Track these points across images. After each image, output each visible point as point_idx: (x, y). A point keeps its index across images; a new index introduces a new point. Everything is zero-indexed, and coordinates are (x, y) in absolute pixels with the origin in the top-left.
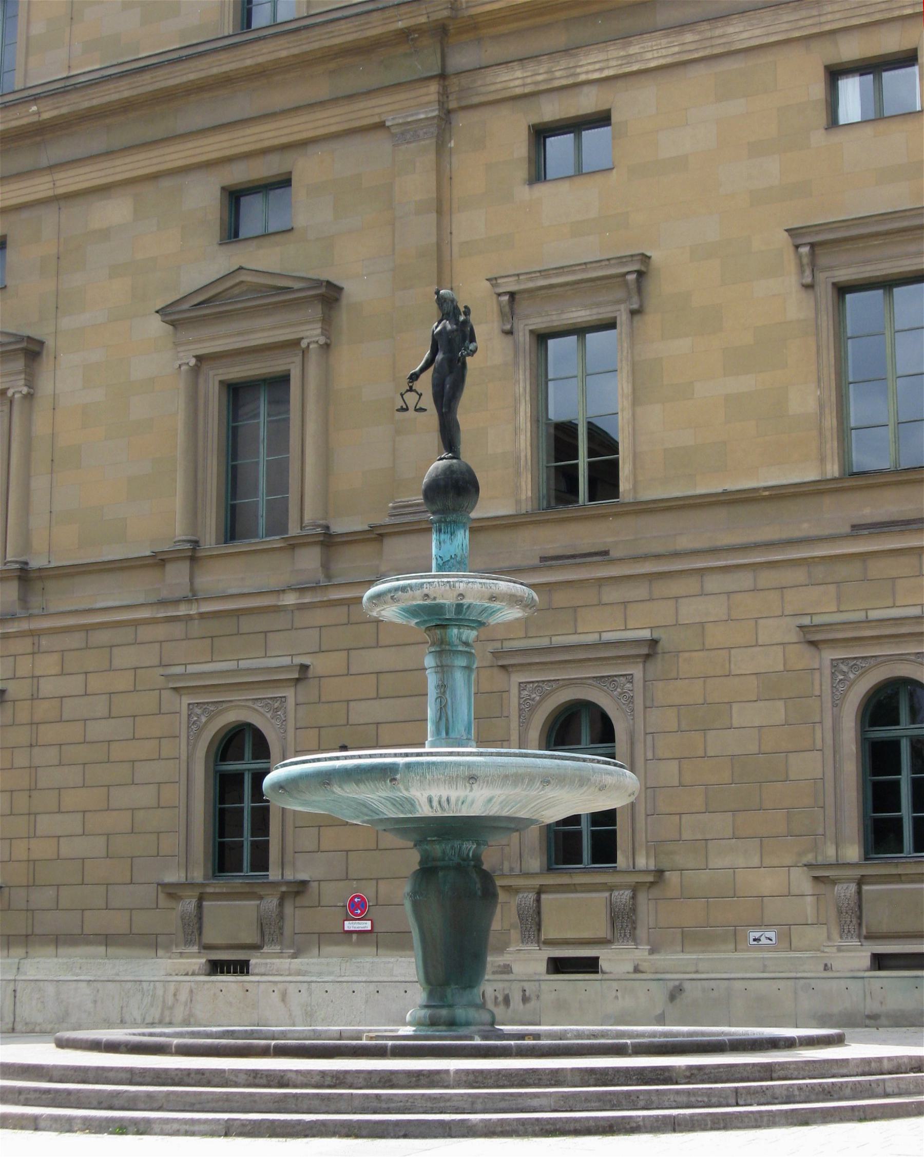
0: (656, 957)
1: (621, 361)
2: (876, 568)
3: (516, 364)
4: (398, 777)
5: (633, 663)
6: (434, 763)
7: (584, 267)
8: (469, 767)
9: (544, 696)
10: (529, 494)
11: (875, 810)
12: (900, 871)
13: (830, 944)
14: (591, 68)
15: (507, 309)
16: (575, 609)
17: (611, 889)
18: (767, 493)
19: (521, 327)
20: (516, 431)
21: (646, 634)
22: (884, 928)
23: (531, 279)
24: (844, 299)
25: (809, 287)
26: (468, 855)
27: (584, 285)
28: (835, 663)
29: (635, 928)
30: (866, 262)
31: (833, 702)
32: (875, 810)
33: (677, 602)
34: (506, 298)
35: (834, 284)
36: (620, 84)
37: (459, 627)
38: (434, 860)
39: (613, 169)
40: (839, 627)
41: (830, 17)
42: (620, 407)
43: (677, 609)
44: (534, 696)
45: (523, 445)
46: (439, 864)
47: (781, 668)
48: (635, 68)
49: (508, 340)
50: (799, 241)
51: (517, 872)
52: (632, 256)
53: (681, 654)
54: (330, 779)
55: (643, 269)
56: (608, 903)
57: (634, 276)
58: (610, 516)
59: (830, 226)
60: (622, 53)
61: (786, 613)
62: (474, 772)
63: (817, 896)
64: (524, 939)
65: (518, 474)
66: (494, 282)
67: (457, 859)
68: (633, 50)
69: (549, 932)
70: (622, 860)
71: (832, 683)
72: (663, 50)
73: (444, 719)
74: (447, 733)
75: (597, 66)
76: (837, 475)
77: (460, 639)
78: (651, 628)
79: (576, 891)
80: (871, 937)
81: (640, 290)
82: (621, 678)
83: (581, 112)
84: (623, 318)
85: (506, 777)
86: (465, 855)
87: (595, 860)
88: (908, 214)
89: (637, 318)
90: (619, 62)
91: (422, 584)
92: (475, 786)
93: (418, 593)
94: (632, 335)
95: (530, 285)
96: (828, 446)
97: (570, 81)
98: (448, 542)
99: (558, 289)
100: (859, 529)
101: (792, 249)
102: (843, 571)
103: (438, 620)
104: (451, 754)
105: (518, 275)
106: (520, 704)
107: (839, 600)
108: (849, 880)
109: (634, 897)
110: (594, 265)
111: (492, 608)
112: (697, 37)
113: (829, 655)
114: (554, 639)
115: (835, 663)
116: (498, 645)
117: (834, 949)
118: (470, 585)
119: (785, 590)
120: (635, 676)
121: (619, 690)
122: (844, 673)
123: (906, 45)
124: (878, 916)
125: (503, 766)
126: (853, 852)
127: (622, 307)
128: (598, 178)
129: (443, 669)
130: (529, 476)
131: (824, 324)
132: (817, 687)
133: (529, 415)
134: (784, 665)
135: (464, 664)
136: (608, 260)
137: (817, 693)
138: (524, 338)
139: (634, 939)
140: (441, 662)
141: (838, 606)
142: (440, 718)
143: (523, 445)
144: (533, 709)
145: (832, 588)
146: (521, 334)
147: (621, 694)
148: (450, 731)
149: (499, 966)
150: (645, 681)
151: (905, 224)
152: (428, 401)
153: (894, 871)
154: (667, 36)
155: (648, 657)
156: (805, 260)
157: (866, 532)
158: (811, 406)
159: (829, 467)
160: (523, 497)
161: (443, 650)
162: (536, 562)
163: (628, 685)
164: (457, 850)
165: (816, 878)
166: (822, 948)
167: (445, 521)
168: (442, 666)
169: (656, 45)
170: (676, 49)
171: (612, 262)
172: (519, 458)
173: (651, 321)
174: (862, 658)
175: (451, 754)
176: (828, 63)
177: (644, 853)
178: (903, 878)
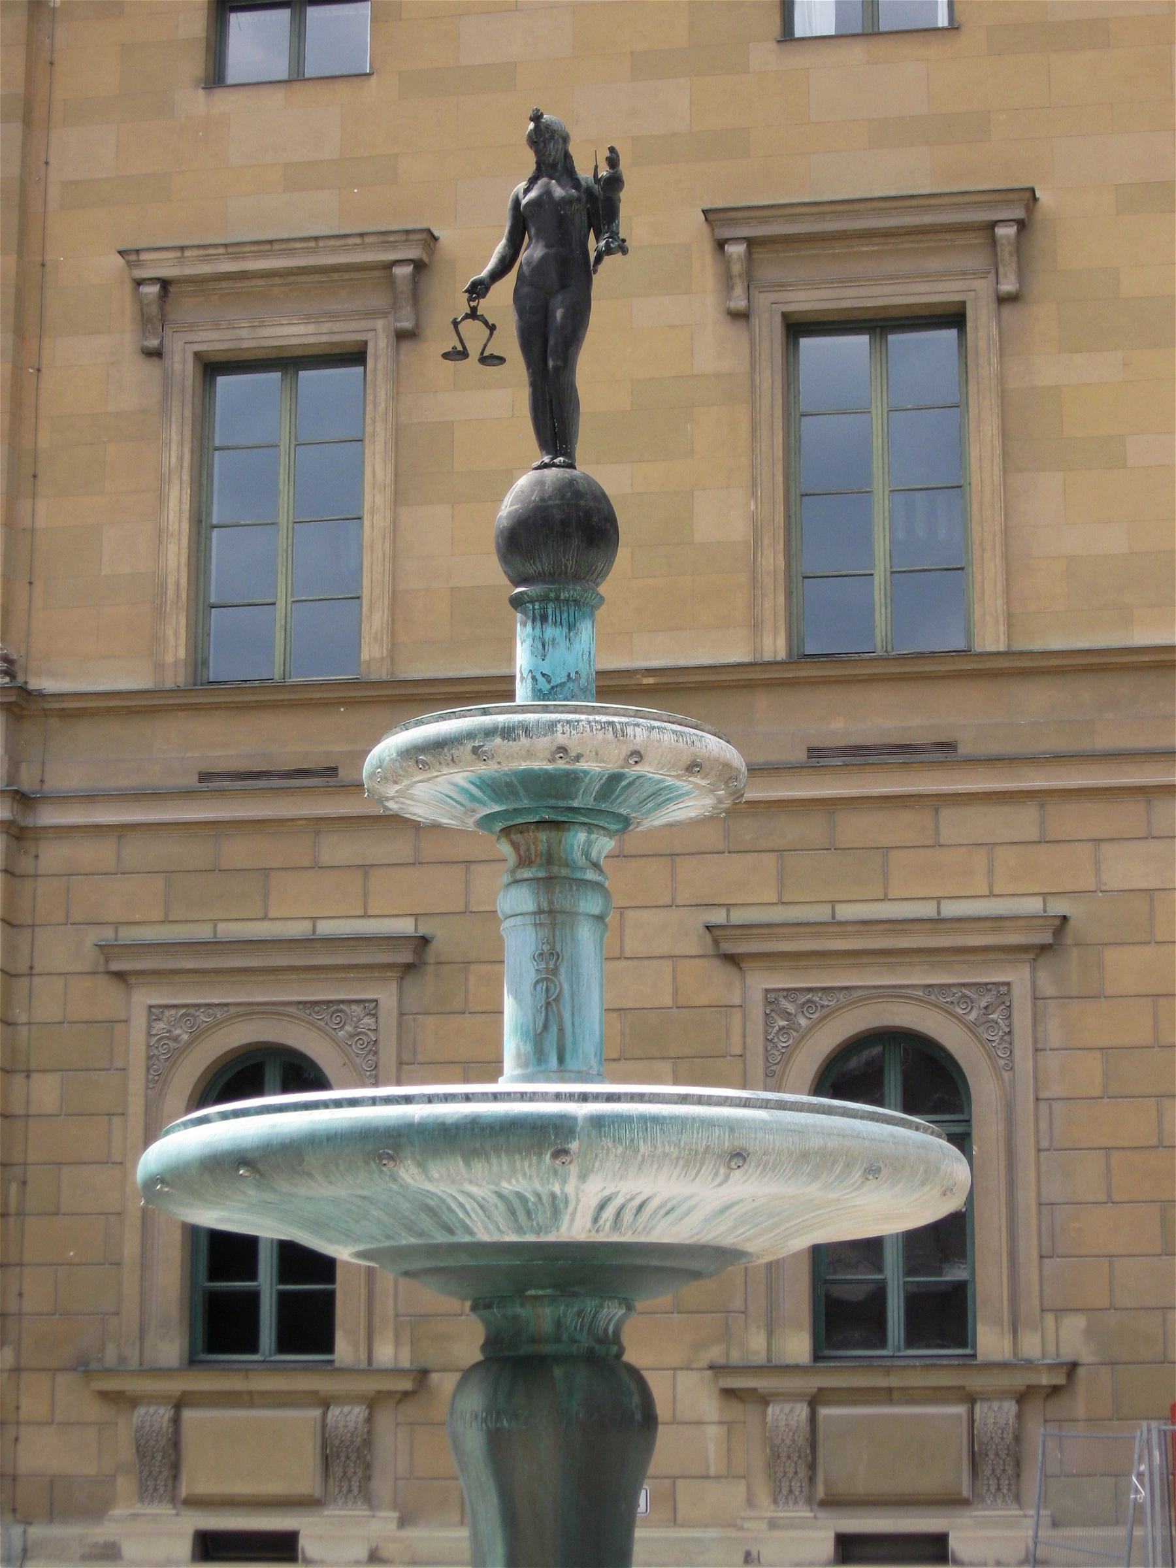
0: (411, 1533)
1: (374, 421)
2: (854, 829)
3: (165, 410)
4: (574, 1146)
5: (345, 979)
6: (655, 1119)
7: (312, 244)
8: (732, 1130)
9: (198, 1035)
10: (182, 654)
11: (212, 1277)
12: (894, 1381)
13: (752, 1514)
15: (154, 310)
16: (266, 872)
17: (325, 1403)
18: (651, 680)
19: (179, 345)
20: (160, 536)
21: (405, 926)
22: (861, 1487)
23: (206, 259)
24: (796, 344)
25: (740, 316)
26: (606, 1330)
27: (304, 278)
28: (771, 996)
29: (369, 1478)
30: (844, 282)
31: (767, 1068)
32: (212, 1277)
33: (467, 870)
34: (155, 289)
35: (785, 316)
37: (590, 828)
38: (533, 1340)
39: (370, 74)
40: (786, 931)
42: (367, 505)
43: (467, 882)
44: (177, 1032)
45: (172, 563)
46: (548, 1349)
47: (668, 1001)
49: (151, 368)
50: (726, 233)
51: (133, 1364)
52: (408, 232)
53: (473, 967)
54: (397, 1148)
55: (426, 259)
56: (319, 1428)
57: (408, 270)
58: (340, 704)
59: (788, 211)
61: (679, 902)
62: (743, 1143)
63: (729, 1426)
64: (146, 1492)
65: (160, 614)
66: (133, 257)
67: (585, 1341)
69: (195, 1481)
70: (344, 1349)
71: (766, 1033)
73: (554, 1029)
74: (561, 1060)
76: (782, 655)
77: (587, 855)
78: (416, 916)
79: (252, 1405)
80: (832, 1503)
82: (354, 1007)
84: (380, 346)
85: (805, 1155)
86: (601, 1332)
87: (286, 1343)
88: (932, 201)
89: (406, 346)
91: (553, 725)
92: (737, 1174)
93: (543, 743)
94: (396, 378)
95: (205, 269)
96: (768, 604)
98: (563, 643)
99: (254, 282)
100: (821, 757)
101: (707, 246)
102: (791, 830)
103: (544, 815)
104: (684, 1099)
105: (182, 249)
106: (149, 1047)
107: (781, 881)
108: (794, 1397)
109: (369, 1420)
110: (332, 242)
111: (678, 788)
113: (761, 981)
114: (221, 927)
115: (771, 998)
116: (108, 934)
117: (764, 1525)
118: (655, 733)
119: (678, 859)
120: (381, 1004)
121: (348, 1028)
122: (787, 1015)
124: (846, 1465)
125: (801, 1131)
126: (798, 1346)
127: (380, 324)
128: (343, 90)
129: (553, 920)
130: (183, 621)
131: (766, 385)
132: (736, 1038)
133: (186, 507)
134: (675, 994)
135: (597, 911)
136: (362, 235)
137: (737, 1050)
138: (182, 365)
139: (367, 1498)
140: (551, 902)
141: (780, 895)
142: (546, 1027)
143: (172, 563)
144: (175, 1057)
145: (769, 860)
146: (177, 358)
147: (352, 1036)
148: (568, 1056)
149: (95, 1545)
150: (401, 1014)
151: (928, 219)
153: (881, 1382)
155: (409, 968)
156: (736, 268)
157: (838, 761)
158: (738, 529)
159: (768, 642)
160: (170, 658)
161: (553, 878)
162: (192, 781)
163: (366, 1020)
164: (587, 1320)
165: (729, 1394)
166: (739, 1522)
167: (557, 599)
168: (551, 912)
171: (368, 240)
172: (163, 587)
174: (823, 989)
175: (684, 1099)
177: (391, 1335)
178: (895, 1395)
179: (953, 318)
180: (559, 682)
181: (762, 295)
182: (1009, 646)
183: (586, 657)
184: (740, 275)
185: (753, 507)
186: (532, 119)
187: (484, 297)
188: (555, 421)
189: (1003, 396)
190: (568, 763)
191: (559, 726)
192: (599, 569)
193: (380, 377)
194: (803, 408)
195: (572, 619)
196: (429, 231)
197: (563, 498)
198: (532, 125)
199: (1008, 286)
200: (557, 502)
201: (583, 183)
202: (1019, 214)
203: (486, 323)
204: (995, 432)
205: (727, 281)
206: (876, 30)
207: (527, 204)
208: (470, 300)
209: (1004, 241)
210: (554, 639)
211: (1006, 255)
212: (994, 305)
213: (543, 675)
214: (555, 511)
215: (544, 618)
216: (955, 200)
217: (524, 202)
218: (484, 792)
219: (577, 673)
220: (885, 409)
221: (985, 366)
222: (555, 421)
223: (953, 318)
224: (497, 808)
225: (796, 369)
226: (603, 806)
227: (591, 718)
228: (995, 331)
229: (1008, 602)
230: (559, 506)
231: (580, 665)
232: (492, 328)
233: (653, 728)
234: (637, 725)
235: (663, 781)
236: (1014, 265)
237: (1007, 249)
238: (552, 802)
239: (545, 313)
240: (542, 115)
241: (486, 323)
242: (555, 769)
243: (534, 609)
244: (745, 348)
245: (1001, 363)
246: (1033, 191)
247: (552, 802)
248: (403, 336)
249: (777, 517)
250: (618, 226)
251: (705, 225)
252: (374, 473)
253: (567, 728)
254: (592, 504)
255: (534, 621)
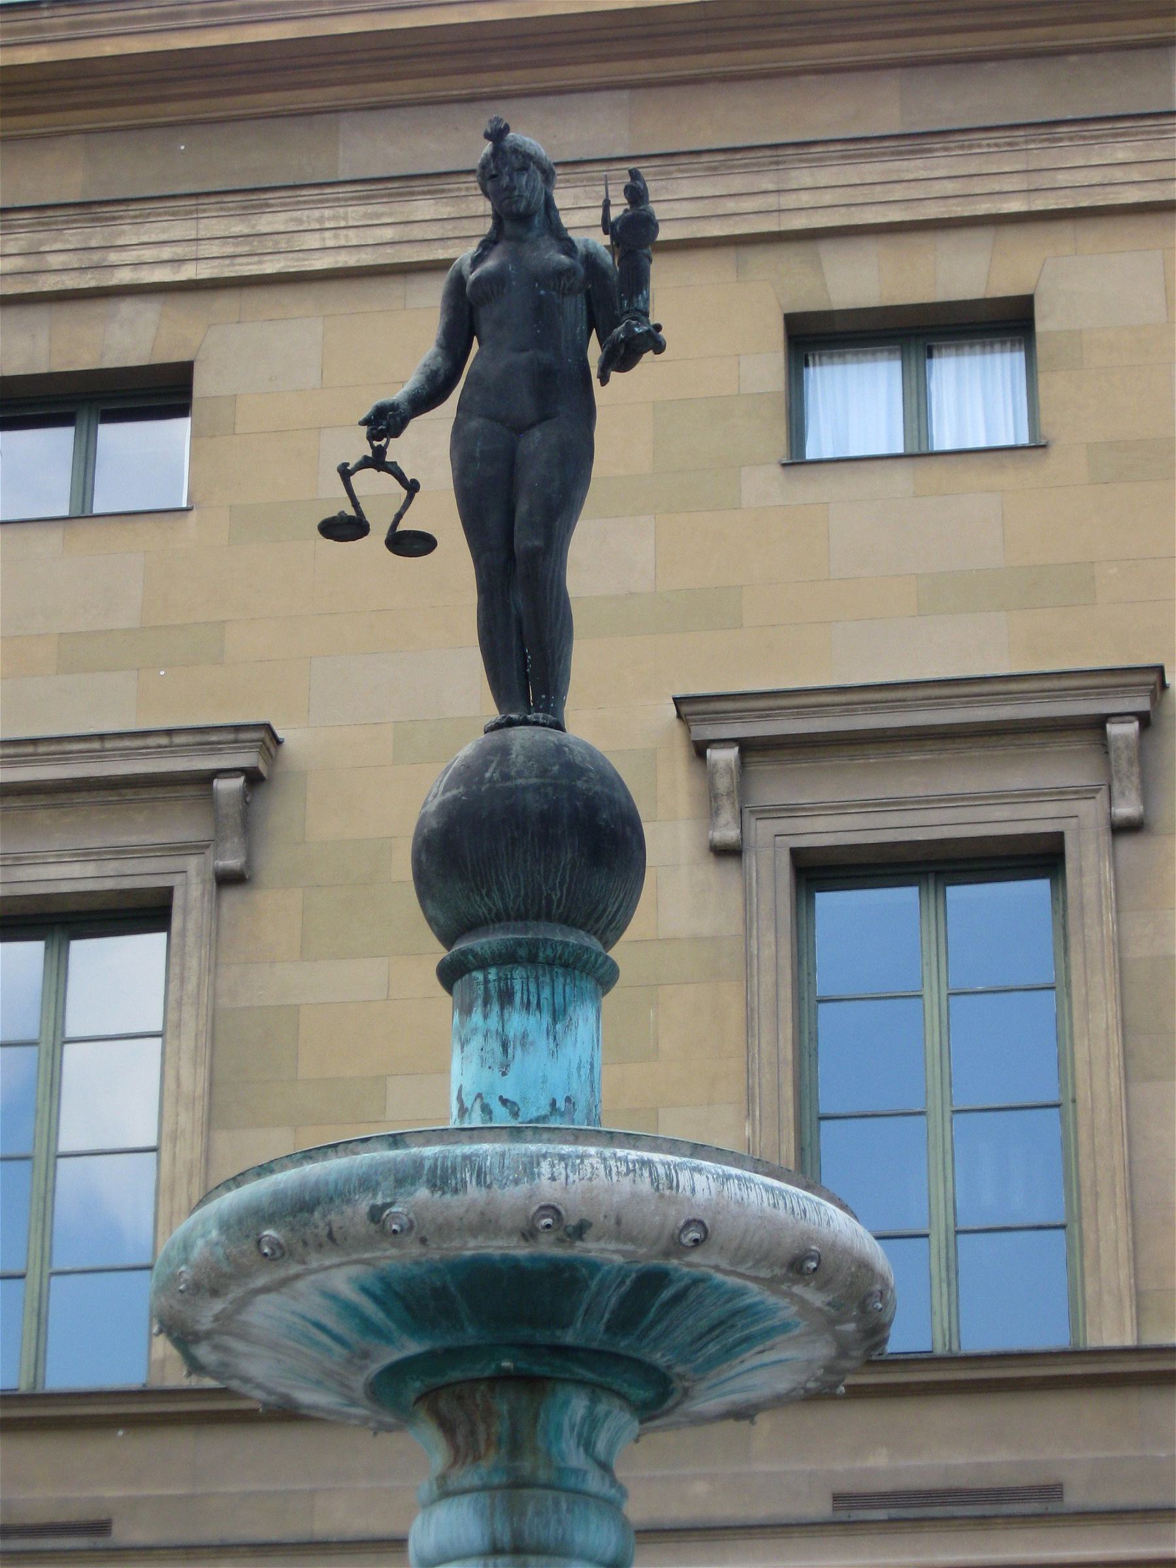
14: (148, 254)
35: (795, 853)
36: (224, 302)
41: (806, 199)
48: (271, 267)
52: (237, 728)
57: (238, 782)
60: (239, 228)
68: (266, 223)
72: (351, 233)
75: (166, 253)
81: (247, 822)
83: (111, 361)
88: (1013, 686)
89: (232, 896)
90: (229, 250)
91: (533, 1162)
94: (215, 938)
97: (88, 281)
98: (543, 1044)
101: (680, 752)
110: (127, 743)
112: (445, 211)
123: (1005, 286)
127: (192, 863)
131: (768, 953)
152: (439, 511)
154: (366, 199)
156: (723, 783)
169: (335, 218)
170: (388, 234)
173: (272, 908)
176: (787, 312)
179: (1041, 858)
180: (534, 1114)
181: (760, 823)
182: (1139, 1339)
183: (585, 1071)
184: (728, 794)
185: (748, 1132)
186: (488, 136)
187: (397, 435)
188: (525, 642)
189: (1122, 968)
190: (560, 1241)
191: (545, 1167)
192: (611, 909)
193: (191, 939)
194: (820, 992)
195: (559, 999)
196: (267, 727)
197: (544, 773)
198: (488, 147)
199: (1127, 809)
200: (533, 781)
201: (580, 247)
202: (1142, 704)
203: (400, 476)
204: (1113, 1021)
205: (710, 803)
206: (924, 450)
207: (478, 280)
208: (371, 437)
209: (1120, 744)
210: (525, 1036)
211: (1124, 764)
212: (1107, 838)
213: (504, 1102)
214: (529, 796)
215: (506, 998)
216: (1047, 684)
217: (472, 277)
218: (388, 1312)
219: (568, 1099)
220: (944, 992)
221: (1094, 928)
222: (525, 642)
223: (1041, 858)
224: (413, 1347)
225: (811, 925)
226: (623, 1345)
227: (608, 1152)
228: (1108, 874)
229: (1136, 1273)
230: (537, 789)
231: (575, 1085)
232: (412, 487)
233: (728, 1177)
234: (699, 1170)
235: (738, 1293)
236: (1135, 779)
237: (1124, 756)
238: (524, 1333)
239: (510, 464)
240: (507, 129)
241: (400, 476)
242: (532, 1259)
243: (486, 981)
244: (735, 899)
245: (1118, 921)
246: (1160, 670)
247: (524, 1333)
248: (228, 880)
249: (784, 1148)
250: (647, 301)
251: (676, 723)
252: (178, 1079)
253: (560, 1168)
254: (598, 788)
255: (486, 1002)
